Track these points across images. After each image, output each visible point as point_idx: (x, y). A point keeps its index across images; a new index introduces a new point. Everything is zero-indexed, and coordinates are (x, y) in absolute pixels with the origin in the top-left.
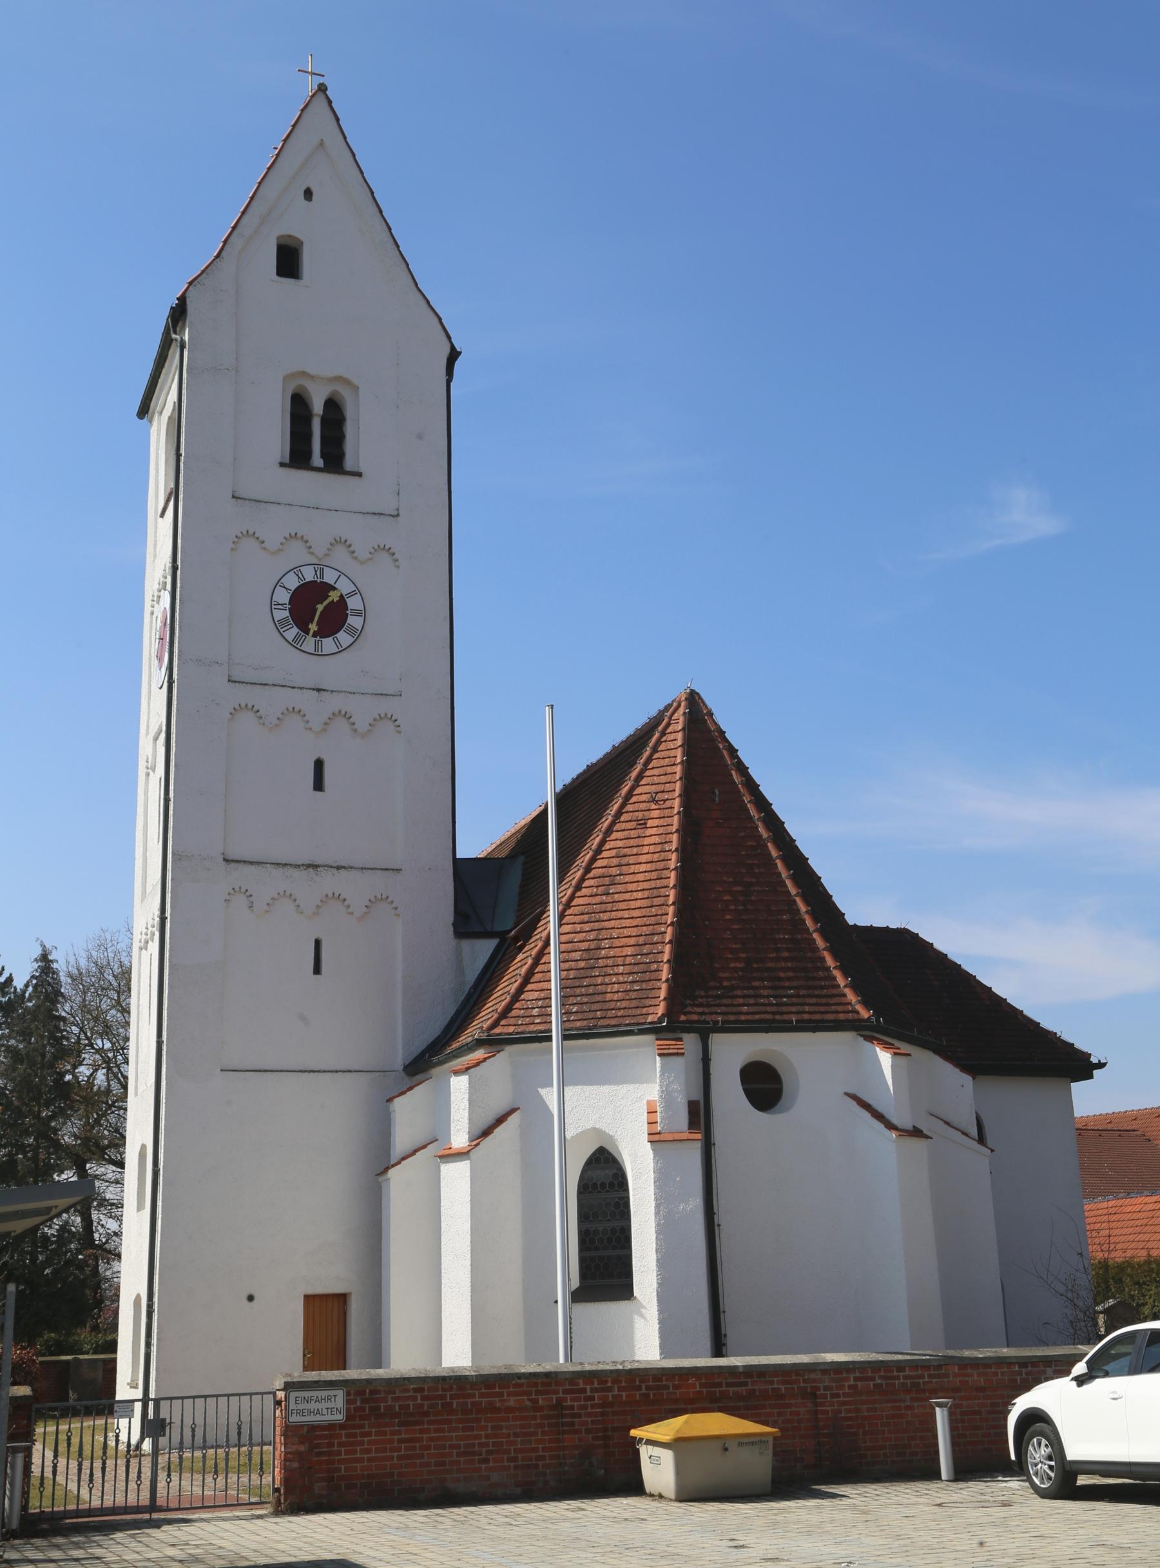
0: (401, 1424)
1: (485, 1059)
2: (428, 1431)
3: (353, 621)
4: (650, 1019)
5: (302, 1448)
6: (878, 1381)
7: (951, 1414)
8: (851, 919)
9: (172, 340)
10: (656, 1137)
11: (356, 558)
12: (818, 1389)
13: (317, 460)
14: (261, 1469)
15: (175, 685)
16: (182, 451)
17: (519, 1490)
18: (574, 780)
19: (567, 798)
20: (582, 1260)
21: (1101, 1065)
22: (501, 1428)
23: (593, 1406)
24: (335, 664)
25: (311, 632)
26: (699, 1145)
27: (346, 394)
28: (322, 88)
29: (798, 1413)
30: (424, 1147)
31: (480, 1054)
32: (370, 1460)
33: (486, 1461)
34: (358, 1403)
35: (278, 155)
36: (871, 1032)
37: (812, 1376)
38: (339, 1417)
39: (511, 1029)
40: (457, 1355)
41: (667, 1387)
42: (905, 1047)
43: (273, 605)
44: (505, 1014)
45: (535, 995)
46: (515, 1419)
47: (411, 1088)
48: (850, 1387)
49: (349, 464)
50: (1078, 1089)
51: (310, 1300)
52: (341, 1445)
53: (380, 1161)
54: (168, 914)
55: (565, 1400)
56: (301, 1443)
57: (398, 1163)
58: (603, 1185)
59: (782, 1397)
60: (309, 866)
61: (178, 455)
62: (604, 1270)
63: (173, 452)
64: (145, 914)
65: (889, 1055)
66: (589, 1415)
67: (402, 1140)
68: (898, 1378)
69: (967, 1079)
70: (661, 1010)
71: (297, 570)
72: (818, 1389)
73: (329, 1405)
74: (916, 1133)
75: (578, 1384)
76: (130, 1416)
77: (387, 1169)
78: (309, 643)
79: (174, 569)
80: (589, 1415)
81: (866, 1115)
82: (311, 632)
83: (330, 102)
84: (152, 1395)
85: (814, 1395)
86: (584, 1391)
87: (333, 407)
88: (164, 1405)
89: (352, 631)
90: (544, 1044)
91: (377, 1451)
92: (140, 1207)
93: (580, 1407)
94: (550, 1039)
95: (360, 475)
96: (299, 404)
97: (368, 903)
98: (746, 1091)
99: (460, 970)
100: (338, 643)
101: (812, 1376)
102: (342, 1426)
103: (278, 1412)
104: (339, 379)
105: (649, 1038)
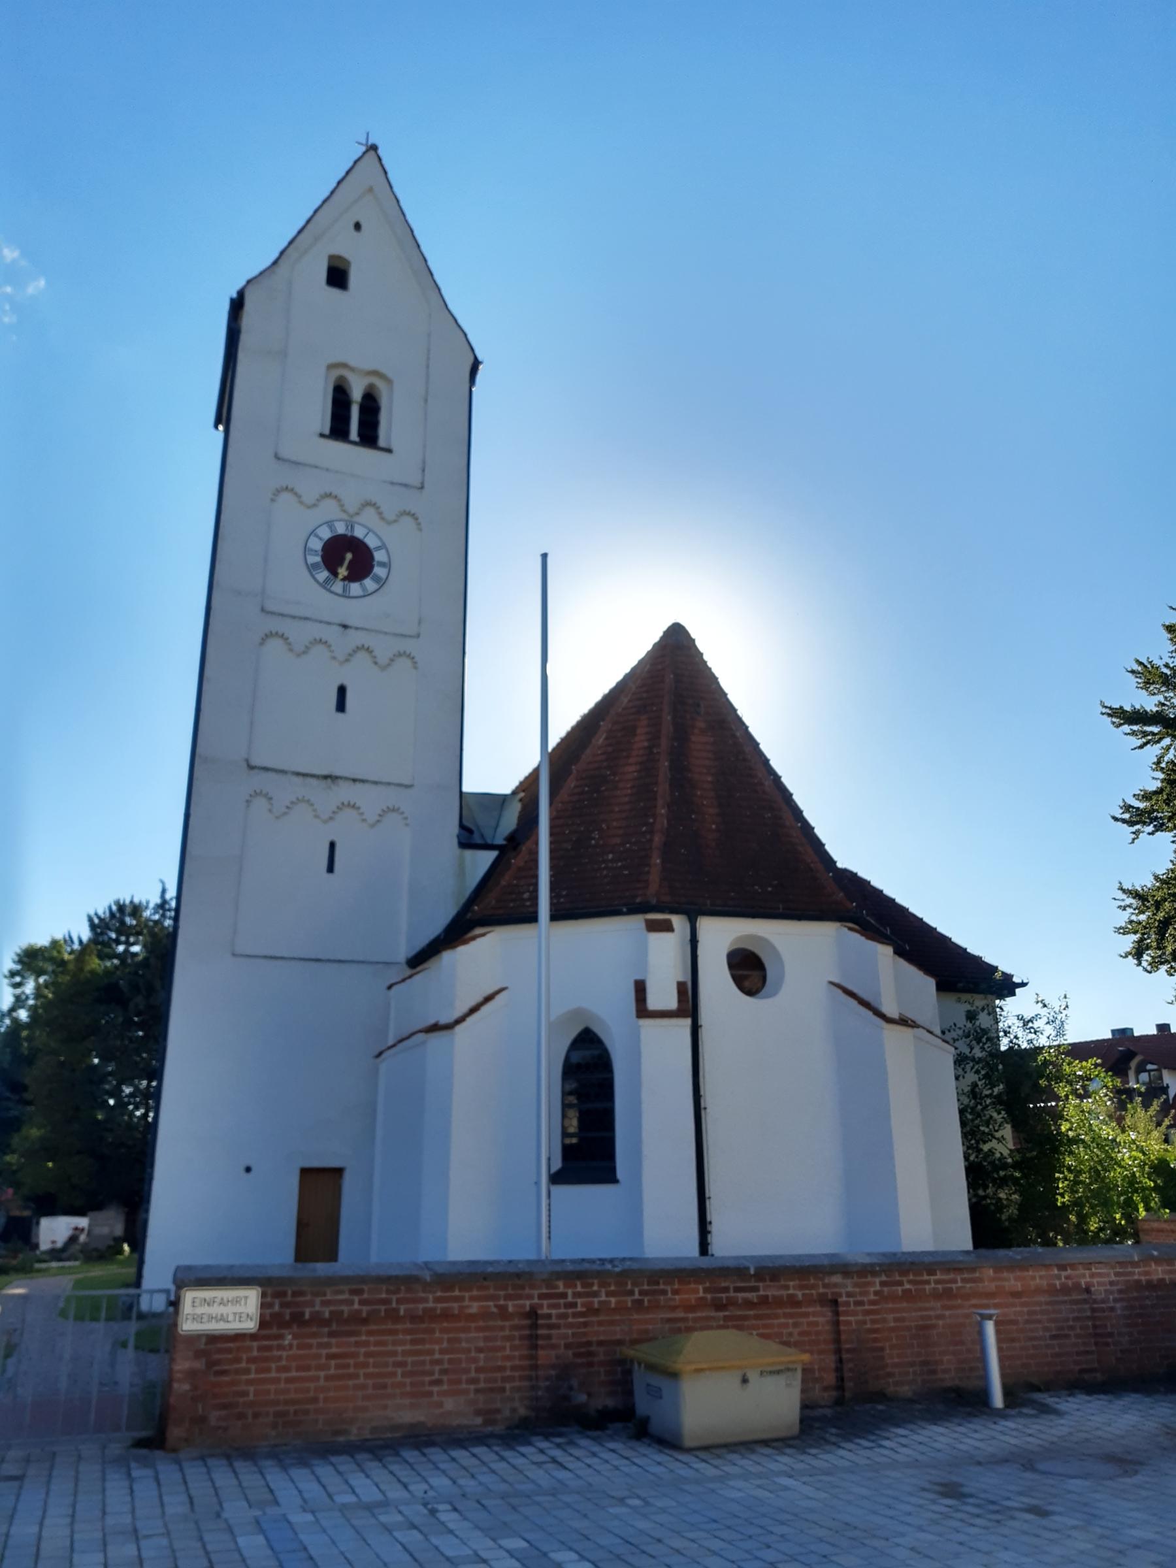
0: (331, 1334)
2: (366, 1344)
6: (907, 1286)
12: (840, 1295)
13: (354, 434)
21: (1023, 985)
22: (459, 1340)
23: (575, 1315)
24: (360, 604)
25: (340, 576)
27: (381, 385)
29: (816, 1324)
32: (289, 1380)
33: (438, 1382)
34: (277, 1308)
38: (251, 1326)
41: (664, 1292)
43: (306, 550)
46: (479, 1329)
47: (410, 977)
48: (876, 1293)
49: (382, 442)
52: (250, 1360)
55: (541, 1306)
59: (798, 1304)
60: (326, 777)
66: (571, 1326)
68: (928, 1282)
71: (330, 524)
72: (840, 1295)
73: (238, 1309)
75: (557, 1287)
78: (338, 586)
80: (571, 1326)
82: (340, 576)
83: (380, 159)
85: (835, 1303)
86: (564, 1295)
89: (377, 579)
91: (299, 1369)
93: (560, 1316)
95: (389, 451)
96: (340, 397)
99: (461, 871)
100: (364, 588)
102: (253, 1337)
104: (375, 373)
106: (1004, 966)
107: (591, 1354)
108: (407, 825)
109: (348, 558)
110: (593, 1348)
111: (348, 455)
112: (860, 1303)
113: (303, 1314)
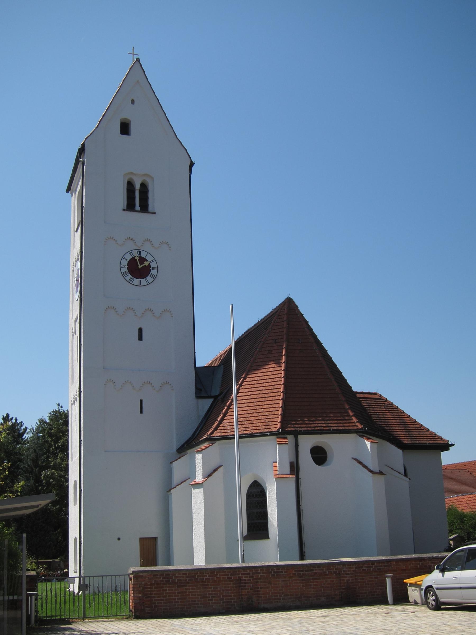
0: (178, 587)
1: (209, 446)
3: (153, 272)
4: (274, 430)
5: (140, 595)
6: (364, 568)
7: (392, 580)
8: (355, 389)
9: (79, 161)
10: (277, 476)
11: (154, 247)
13: (138, 208)
14: (125, 603)
15: (83, 299)
16: (84, 205)
17: (224, 611)
18: (242, 335)
19: (239, 343)
20: (248, 524)
21: (452, 445)
26: (294, 479)
28: (138, 60)
30: (185, 481)
31: (206, 444)
33: (211, 600)
35: (120, 87)
36: (362, 433)
37: (339, 567)
39: (219, 435)
40: (200, 560)
42: (376, 440)
44: (216, 429)
45: (228, 421)
47: (179, 458)
48: (353, 571)
49: (150, 209)
50: (444, 454)
51: (142, 540)
53: (169, 487)
54: (82, 390)
56: (140, 593)
57: (175, 487)
58: (256, 495)
61: (82, 207)
62: (257, 527)
63: (81, 206)
64: (74, 389)
65: (369, 443)
66: (251, 583)
67: (176, 478)
69: (400, 451)
70: (279, 426)
71: (130, 252)
72: (341, 572)
74: (380, 473)
76: (74, 583)
77: (171, 489)
79: (81, 252)
81: (361, 466)
83: (141, 65)
84: (82, 575)
86: (249, 574)
87: (144, 187)
88: (87, 579)
90: (232, 440)
92: (75, 504)
93: (248, 580)
94: (234, 438)
95: (155, 213)
96: (130, 185)
97: (161, 385)
98: (313, 458)
100: (147, 281)
101: (339, 567)
103: (130, 582)
104: (146, 175)
105: (275, 437)
106: (445, 437)
107: (258, 591)
108: (173, 390)
109: (138, 269)
110: (260, 589)
111: (136, 217)
112: (348, 574)
113: (170, 581)
